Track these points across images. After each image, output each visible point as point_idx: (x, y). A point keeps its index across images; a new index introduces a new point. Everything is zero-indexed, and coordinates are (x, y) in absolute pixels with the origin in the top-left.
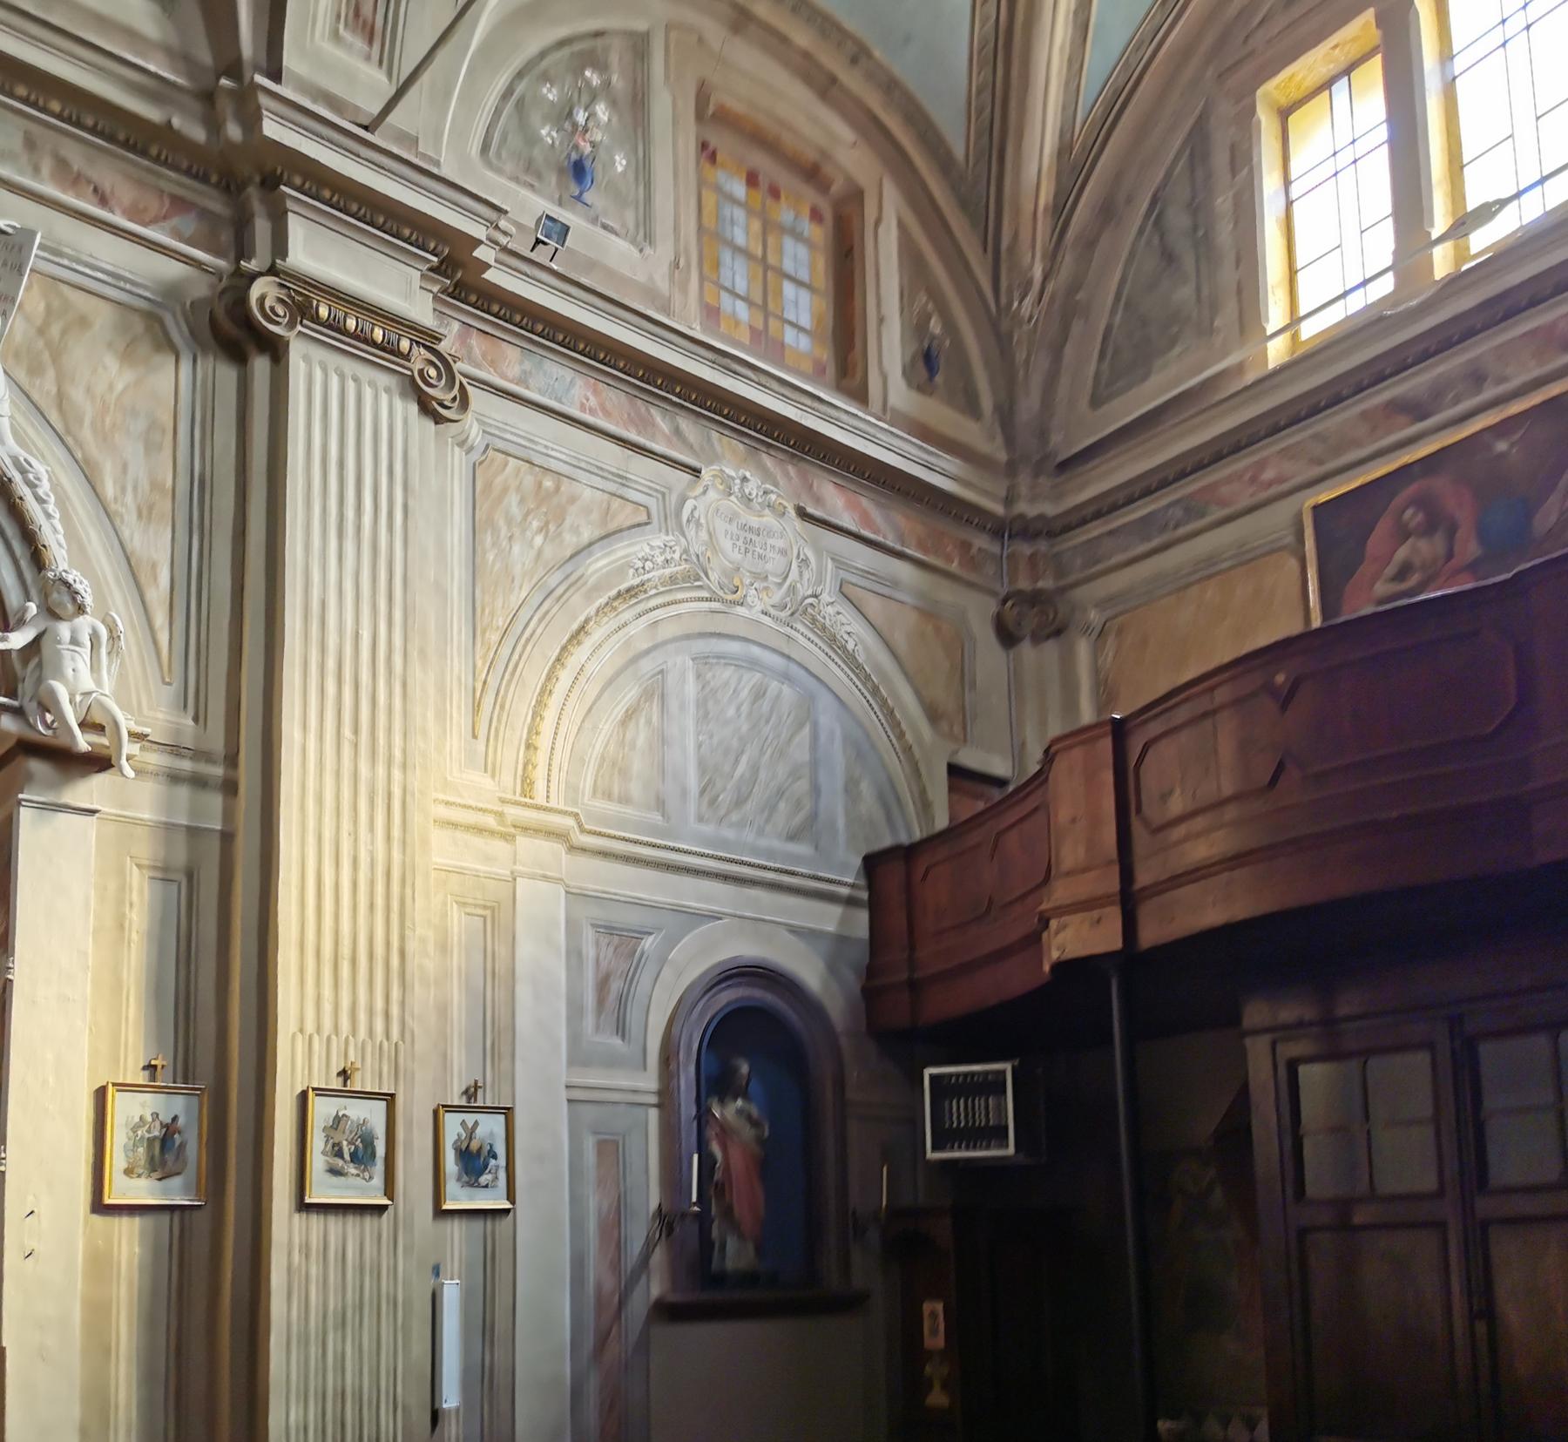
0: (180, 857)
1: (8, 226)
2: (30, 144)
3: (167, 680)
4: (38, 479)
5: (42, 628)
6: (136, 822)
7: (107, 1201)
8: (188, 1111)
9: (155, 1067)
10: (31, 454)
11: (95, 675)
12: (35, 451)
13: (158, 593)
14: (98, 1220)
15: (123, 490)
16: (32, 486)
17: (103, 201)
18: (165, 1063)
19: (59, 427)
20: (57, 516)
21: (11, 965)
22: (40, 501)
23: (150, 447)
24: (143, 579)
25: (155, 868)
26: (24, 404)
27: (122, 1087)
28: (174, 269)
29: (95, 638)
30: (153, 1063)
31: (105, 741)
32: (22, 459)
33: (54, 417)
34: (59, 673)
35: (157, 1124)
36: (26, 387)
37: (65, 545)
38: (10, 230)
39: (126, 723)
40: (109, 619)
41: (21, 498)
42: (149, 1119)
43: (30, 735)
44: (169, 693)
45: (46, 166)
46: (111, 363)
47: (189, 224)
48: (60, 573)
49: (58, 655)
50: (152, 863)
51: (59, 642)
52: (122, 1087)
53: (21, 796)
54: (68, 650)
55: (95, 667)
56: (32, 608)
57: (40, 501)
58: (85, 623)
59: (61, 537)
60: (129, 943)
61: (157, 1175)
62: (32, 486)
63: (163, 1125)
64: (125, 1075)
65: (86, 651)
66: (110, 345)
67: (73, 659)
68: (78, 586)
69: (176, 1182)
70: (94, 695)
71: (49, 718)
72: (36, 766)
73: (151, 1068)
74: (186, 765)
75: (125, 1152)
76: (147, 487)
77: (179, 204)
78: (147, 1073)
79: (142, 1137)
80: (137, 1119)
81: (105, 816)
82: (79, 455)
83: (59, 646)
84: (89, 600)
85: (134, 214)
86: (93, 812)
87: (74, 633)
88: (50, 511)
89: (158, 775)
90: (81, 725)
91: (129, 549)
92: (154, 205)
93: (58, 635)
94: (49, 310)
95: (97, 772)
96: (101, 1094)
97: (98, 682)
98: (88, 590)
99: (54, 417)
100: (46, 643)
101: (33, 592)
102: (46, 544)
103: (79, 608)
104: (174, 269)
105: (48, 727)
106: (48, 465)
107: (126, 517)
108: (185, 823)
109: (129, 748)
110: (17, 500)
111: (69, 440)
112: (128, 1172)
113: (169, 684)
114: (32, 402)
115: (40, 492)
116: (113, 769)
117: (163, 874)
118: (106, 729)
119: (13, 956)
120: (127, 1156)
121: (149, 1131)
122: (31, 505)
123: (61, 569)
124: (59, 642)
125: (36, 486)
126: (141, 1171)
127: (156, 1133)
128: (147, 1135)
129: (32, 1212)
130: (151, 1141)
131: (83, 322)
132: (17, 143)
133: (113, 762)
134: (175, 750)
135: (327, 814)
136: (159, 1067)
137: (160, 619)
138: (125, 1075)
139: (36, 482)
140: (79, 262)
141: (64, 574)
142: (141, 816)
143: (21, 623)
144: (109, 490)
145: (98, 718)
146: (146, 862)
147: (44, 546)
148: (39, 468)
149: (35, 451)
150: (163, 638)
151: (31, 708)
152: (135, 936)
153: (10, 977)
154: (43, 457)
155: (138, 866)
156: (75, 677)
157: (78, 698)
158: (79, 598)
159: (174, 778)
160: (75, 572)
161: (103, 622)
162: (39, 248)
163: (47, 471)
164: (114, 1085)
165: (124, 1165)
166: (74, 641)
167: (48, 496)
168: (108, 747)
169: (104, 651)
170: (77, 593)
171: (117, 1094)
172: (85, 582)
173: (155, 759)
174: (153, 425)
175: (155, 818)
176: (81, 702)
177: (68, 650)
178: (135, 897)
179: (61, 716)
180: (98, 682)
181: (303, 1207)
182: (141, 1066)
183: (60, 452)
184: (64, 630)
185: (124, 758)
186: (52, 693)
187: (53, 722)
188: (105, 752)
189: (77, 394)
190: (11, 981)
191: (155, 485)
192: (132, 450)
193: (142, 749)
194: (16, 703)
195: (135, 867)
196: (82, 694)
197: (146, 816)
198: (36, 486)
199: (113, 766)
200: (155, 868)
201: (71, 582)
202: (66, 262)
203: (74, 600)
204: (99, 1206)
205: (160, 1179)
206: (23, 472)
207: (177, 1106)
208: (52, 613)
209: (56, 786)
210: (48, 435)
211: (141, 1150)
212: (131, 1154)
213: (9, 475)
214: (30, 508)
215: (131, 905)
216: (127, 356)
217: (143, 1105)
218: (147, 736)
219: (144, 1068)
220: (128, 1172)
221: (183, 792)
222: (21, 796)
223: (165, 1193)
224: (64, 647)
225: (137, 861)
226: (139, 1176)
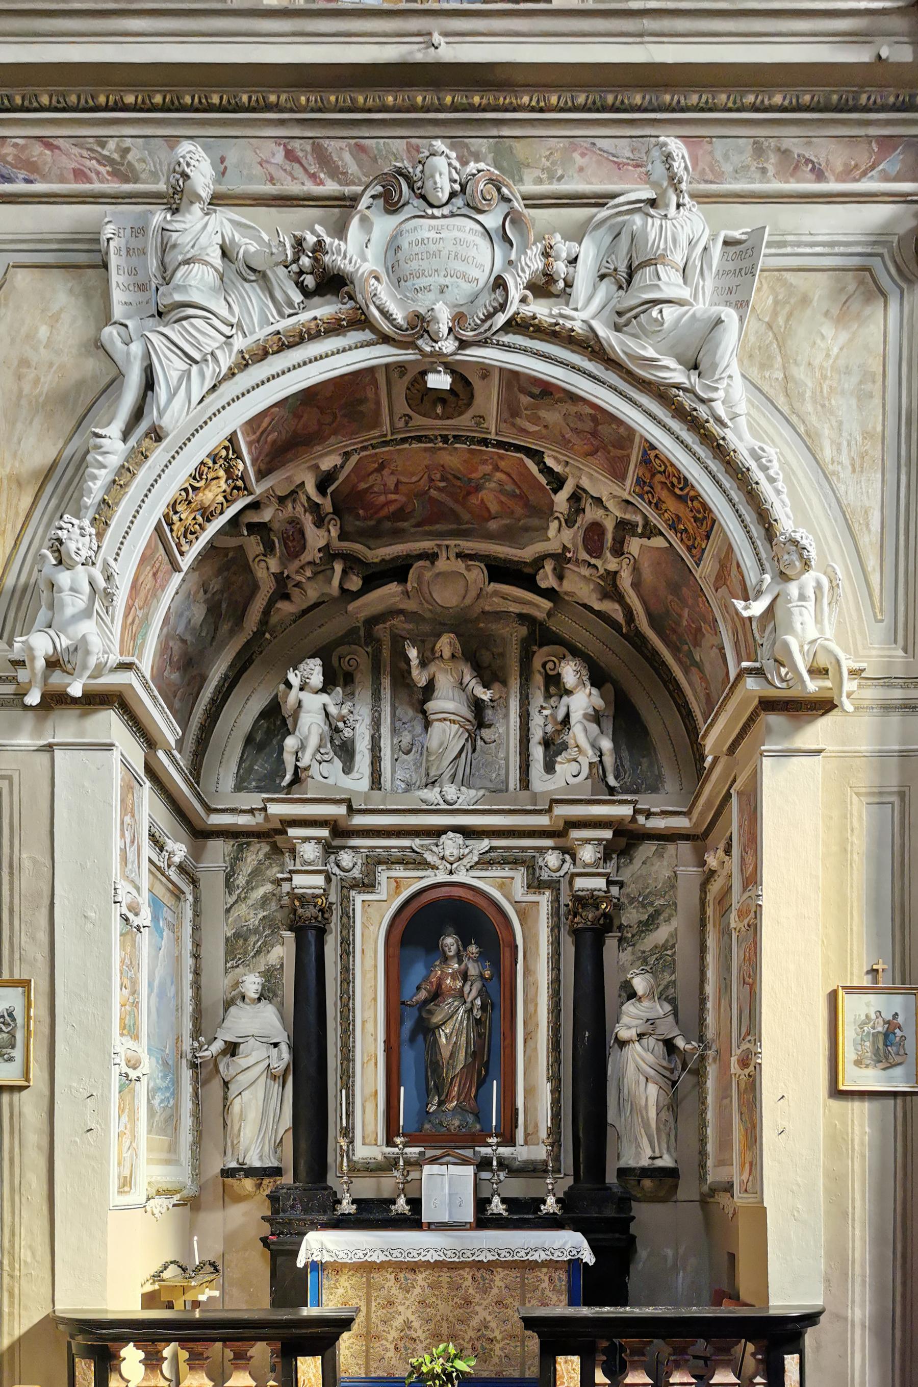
0: (893, 782)
1: (743, 233)
2: (759, 151)
3: (879, 617)
4: (770, 461)
5: (775, 594)
6: (856, 755)
7: (841, 1088)
8: (906, 1008)
9: (877, 971)
10: (764, 442)
11: (819, 626)
12: (766, 438)
13: (869, 540)
14: (837, 1105)
15: (839, 450)
16: (764, 469)
17: (820, 176)
18: (886, 967)
19: (785, 409)
20: (785, 490)
21: (760, 893)
22: (772, 480)
23: (862, 397)
24: (856, 527)
25: (872, 794)
26: (758, 399)
27: (851, 990)
28: (879, 214)
29: (819, 587)
30: (875, 967)
31: (828, 684)
32: (756, 448)
33: (781, 401)
34: (790, 630)
35: (881, 1020)
36: (759, 383)
37: (791, 516)
38: (744, 237)
39: (847, 664)
40: (829, 569)
41: (757, 483)
42: (873, 1016)
43: (771, 692)
44: (879, 631)
45: (772, 162)
46: (828, 330)
47: (894, 162)
48: (790, 535)
49: (789, 613)
50: (868, 790)
51: (790, 602)
52: (851, 990)
53: (763, 748)
54: (797, 606)
55: (818, 620)
56: (767, 578)
57: (772, 480)
58: (809, 579)
59: (788, 509)
60: (851, 864)
61: (881, 1065)
62: (764, 469)
63: (885, 1022)
64: (851, 980)
65: (811, 604)
66: (827, 314)
67: (801, 614)
68: (804, 542)
69: (898, 1071)
70: (819, 641)
71: (783, 671)
72: (774, 719)
73: (874, 972)
74: (898, 693)
75: (854, 1045)
76: (859, 438)
77: (887, 143)
78: (870, 976)
79: (868, 1033)
80: (863, 1017)
81: (829, 754)
82: (802, 429)
83: (789, 605)
84: (813, 554)
85: (847, 174)
86: (819, 752)
87: (801, 588)
88: (780, 488)
89: (873, 708)
90: (810, 672)
91: (844, 502)
92: (863, 158)
93: (789, 595)
94: (776, 302)
95: (823, 715)
96: (833, 997)
97: (822, 631)
98: (813, 543)
99: (781, 401)
100: (779, 612)
101: (767, 566)
102: (777, 517)
103: (806, 564)
104: (879, 214)
105: (783, 680)
106: (778, 447)
107: (842, 475)
108: (897, 748)
109: (850, 685)
110: (754, 486)
111: (794, 419)
112: (858, 1063)
113: (882, 621)
114: (763, 394)
115: (771, 472)
116: (836, 710)
117: (879, 798)
118: (830, 672)
119: (761, 885)
120: (856, 1049)
121: (874, 1028)
122: (766, 489)
123: (790, 530)
124: (790, 602)
125: (768, 468)
126: (869, 1062)
127: (880, 1029)
128: (872, 1031)
129: (783, 1097)
130: (875, 1035)
131: (805, 301)
132: (747, 157)
133: (835, 702)
134: (886, 681)
135: (710, 1077)
136: (880, 970)
137: (872, 563)
138: (851, 980)
139: (768, 464)
140: (799, 244)
141: (793, 534)
142: (858, 748)
143: (759, 594)
144: (828, 453)
145: (823, 661)
146: (863, 790)
147: (775, 520)
148: (771, 451)
149: (766, 438)
150: (875, 579)
151: (768, 665)
152: (856, 857)
153: (760, 903)
154: (773, 441)
155: (857, 794)
156: (803, 630)
157: (806, 647)
158: (805, 553)
159: (886, 708)
160: (801, 530)
161: (825, 573)
162: (767, 247)
163: (776, 453)
164: (844, 988)
165: (854, 1057)
166: (802, 597)
167: (778, 474)
168: (831, 689)
169: (825, 601)
170: (804, 548)
171: (846, 996)
172: (811, 537)
173: (871, 694)
174: (867, 376)
175: (870, 748)
176: (808, 650)
177: (797, 606)
178: (856, 824)
179: (794, 668)
180: (822, 631)
181: (25, 984)
182: (865, 970)
183: (787, 432)
184: (793, 589)
185: (844, 695)
186: (786, 646)
187: (787, 674)
188: (827, 694)
189: (799, 373)
190: (761, 906)
191: (867, 435)
192: (845, 407)
193: (860, 686)
194: (757, 665)
195: (854, 796)
196: (809, 643)
197: (863, 748)
198: (768, 468)
199: (836, 706)
200: (872, 794)
201: (799, 539)
202: (789, 250)
203: (801, 555)
204: (837, 1093)
205: (884, 1069)
206: (757, 458)
207: (896, 1004)
208: (783, 577)
209: (788, 735)
210: (777, 420)
211: (867, 1044)
212: (859, 1047)
213: (747, 465)
214: (763, 490)
215: (852, 830)
216: (841, 319)
217: (868, 1005)
218: (863, 670)
219: (868, 973)
220: (858, 1063)
221: (895, 719)
222: (763, 748)
223: (890, 1079)
224: (794, 604)
225: (856, 790)
226: (867, 1066)
